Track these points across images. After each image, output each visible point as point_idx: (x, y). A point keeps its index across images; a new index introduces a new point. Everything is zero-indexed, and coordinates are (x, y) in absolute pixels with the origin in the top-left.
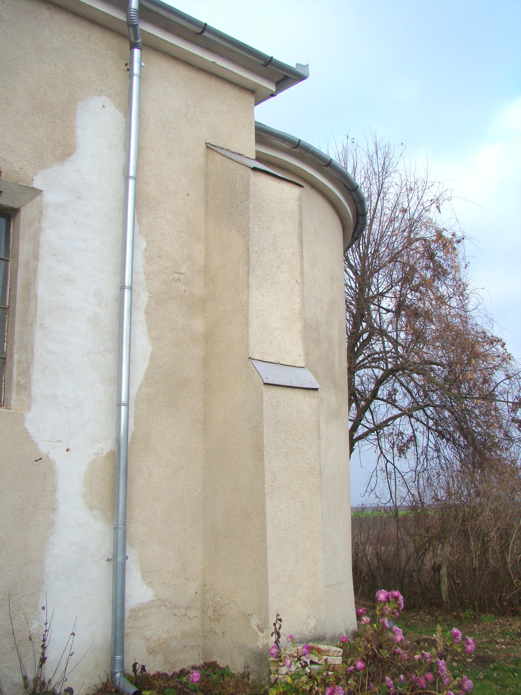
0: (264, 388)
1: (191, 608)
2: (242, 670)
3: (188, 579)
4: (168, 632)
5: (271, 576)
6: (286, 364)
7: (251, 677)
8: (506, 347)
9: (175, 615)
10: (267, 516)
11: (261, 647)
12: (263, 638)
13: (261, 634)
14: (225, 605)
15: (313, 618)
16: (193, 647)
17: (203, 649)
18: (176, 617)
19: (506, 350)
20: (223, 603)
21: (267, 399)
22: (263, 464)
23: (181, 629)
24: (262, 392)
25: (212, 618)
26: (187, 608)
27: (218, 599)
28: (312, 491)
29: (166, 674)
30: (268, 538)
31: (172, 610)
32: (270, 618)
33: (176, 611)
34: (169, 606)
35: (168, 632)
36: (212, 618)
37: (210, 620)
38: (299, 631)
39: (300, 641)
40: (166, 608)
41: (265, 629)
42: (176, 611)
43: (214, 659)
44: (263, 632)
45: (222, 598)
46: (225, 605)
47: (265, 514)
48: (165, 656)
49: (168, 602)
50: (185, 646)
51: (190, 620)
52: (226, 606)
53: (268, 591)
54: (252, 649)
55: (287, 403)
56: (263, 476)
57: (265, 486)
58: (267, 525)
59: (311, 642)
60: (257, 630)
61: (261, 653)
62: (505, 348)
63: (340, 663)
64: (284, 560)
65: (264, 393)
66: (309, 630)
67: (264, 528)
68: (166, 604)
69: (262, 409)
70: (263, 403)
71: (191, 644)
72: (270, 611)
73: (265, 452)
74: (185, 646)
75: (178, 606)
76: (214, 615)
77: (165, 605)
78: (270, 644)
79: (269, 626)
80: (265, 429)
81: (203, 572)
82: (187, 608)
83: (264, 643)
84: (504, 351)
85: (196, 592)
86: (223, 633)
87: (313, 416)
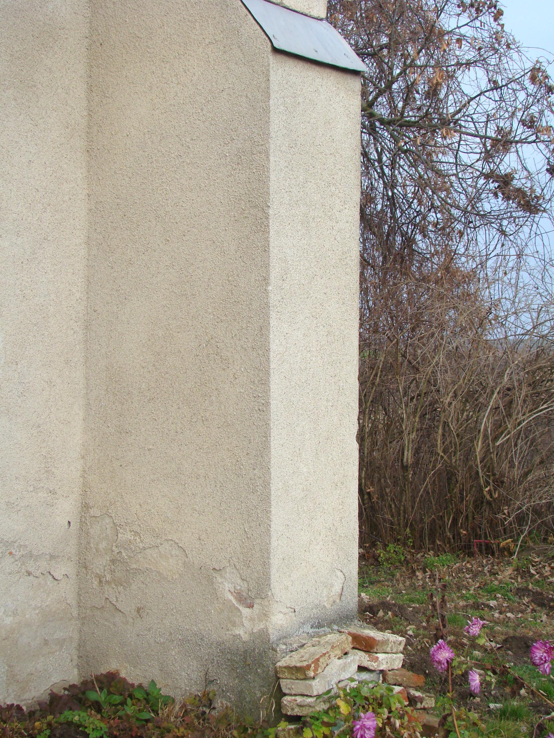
0: (273, 60)
1: (58, 556)
2: (197, 690)
3: (53, 492)
4: (15, 613)
5: (276, 486)
6: (293, 7)
7: (218, 703)
8: (504, 20)
9: (29, 574)
10: (272, 354)
11: (245, 637)
12: (252, 619)
13: (246, 611)
14: (145, 549)
15: (339, 574)
16: (61, 643)
17: (81, 646)
18: (31, 577)
19: (502, 26)
20: (141, 545)
21: (276, 89)
22: (267, 240)
23: (39, 605)
24: (268, 70)
25: (108, 577)
26: (52, 557)
27: (126, 536)
28: (344, 303)
29: (19, 708)
30: (273, 408)
31: (23, 564)
32: (272, 577)
33: (31, 566)
34: (18, 554)
35: (15, 613)
36: (108, 577)
37: (101, 582)
38: (317, 602)
39: (319, 623)
40: (13, 560)
41: (258, 601)
42: (31, 566)
43: (112, 666)
44: (251, 606)
45: (137, 533)
46: (145, 549)
47: (268, 350)
48: (10, 666)
49: (16, 545)
50: (46, 642)
51: (56, 582)
52: (148, 550)
53: (269, 518)
54: (219, 644)
55: (310, 100)
56: (267, 266)
57: (270, 288)
58: (272, 374)
59: (335, 624)
60: (234, 601)
61: (245, 652)
62: (501, 22)
63: (398, 664)
64: (297, 451)
65: (272, 72)
66: (331, 599)
67: (265, 382)
68: (14, 551)
69: (267, 110)
70: (269, 98)
71: (56, 636)
72: (272, 561)
73: (271, 212)
74: (46, 642)
75: (35, 553)
76: (112, 572)
77: (11, 553)
78: (270, 631)
79: (270, 594)
80: (272, 159)
81: (82, 476)
82: (52, 557)
83: (255, 631)
84: (499, 28)
85: (69, 522)
86: (138, 610)
87: (350, 136)
